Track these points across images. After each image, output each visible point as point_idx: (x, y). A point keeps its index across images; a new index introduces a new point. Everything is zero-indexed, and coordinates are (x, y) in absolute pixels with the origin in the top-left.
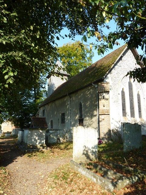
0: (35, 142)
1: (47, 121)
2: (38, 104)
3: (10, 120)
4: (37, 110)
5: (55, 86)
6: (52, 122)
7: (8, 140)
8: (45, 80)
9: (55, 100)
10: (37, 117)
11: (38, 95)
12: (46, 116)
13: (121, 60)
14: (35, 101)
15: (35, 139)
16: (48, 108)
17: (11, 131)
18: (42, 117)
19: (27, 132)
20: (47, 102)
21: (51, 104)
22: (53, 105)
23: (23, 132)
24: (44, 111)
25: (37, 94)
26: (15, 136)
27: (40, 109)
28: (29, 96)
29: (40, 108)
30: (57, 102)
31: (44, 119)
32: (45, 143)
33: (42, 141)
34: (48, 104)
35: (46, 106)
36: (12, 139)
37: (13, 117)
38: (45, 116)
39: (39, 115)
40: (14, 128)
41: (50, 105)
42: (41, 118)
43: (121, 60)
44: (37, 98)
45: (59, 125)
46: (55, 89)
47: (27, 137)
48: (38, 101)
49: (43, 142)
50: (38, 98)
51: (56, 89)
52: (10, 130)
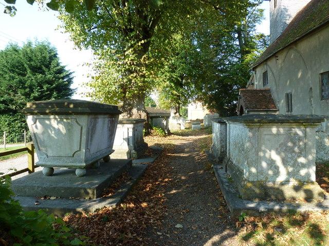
0: (270, 172)
1: (275, 96)
2: (248, 64)
3: (199, 99)
4: (247, 77)
5: (289, 13)
6: (289, 98)
7: (196, 141)
8: (259, 13)
9: (295, 43)
10: (249, 89)
11: (247, 46)
12: (271, 85)
13: (266, 64)
14: (242, 59)
15: (272, 163)
16: (275, 66)
17: (203, 118)
18: (262, 88)
19: (236, 130)
20: (272, 53)
21: (284, 54)
22: (292, 54)
23: (223, 126)
24: (265, 75)
25: (245, 44)
26: (208, 130)
27: (256, 72)
28: (230, 50)
29: (254, 69)
30: (304, 46)
31: (268, 91)
32: (313, 178)
33: (303, 172)
34: (275, 55)
35: (271, 63)
36: (204, 136)
37: (205, 94)
38: (267, 87)
39: (253, 84)
40: (207, 112)
41: (281, 57)
42: (261, 91)
43: (266, 64)
44: (244, 53)
45: (312, 105)
46: (288, 22)
47: (241, 149)
48: (249, 58)
49: (308, 175)
50: (248, 52)
51: (291, 19)
52: (201, 117)
